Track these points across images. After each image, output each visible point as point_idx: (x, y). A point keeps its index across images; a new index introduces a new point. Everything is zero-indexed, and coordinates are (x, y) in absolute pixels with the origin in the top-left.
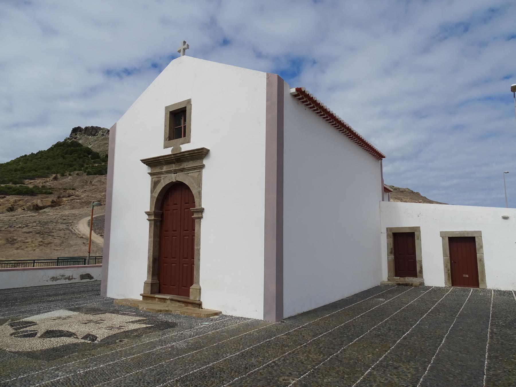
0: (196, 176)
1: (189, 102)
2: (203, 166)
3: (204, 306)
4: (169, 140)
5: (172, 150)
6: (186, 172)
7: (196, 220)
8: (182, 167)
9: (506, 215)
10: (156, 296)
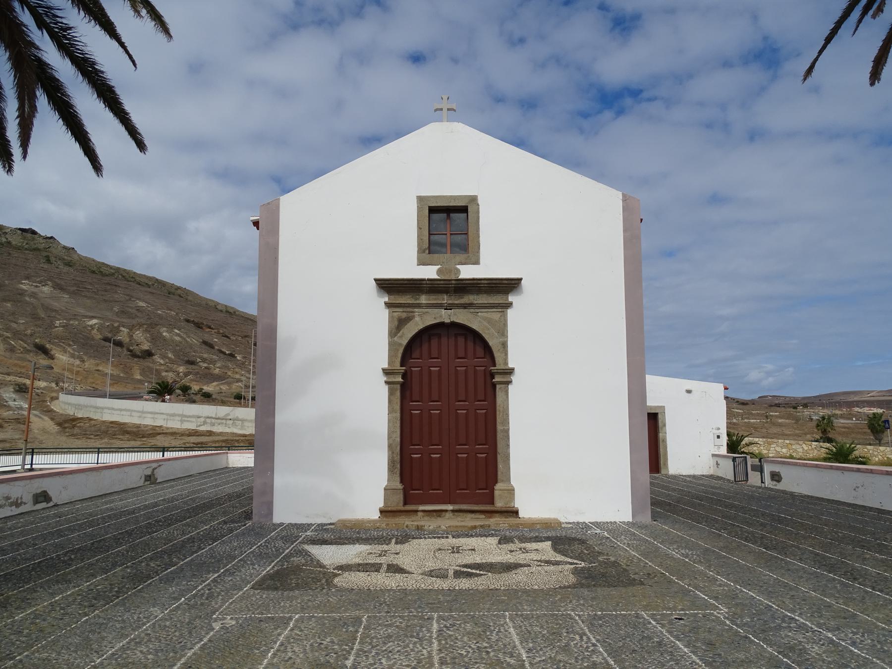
0: (497, 319)
2: (509, 305)
3: (521, 515)
4: (429, 253)
5: (439, 272)
6: (472, 310)
7: (498, 386)
8: (462, 301)
9: (689, 388)
10: (421, 508)
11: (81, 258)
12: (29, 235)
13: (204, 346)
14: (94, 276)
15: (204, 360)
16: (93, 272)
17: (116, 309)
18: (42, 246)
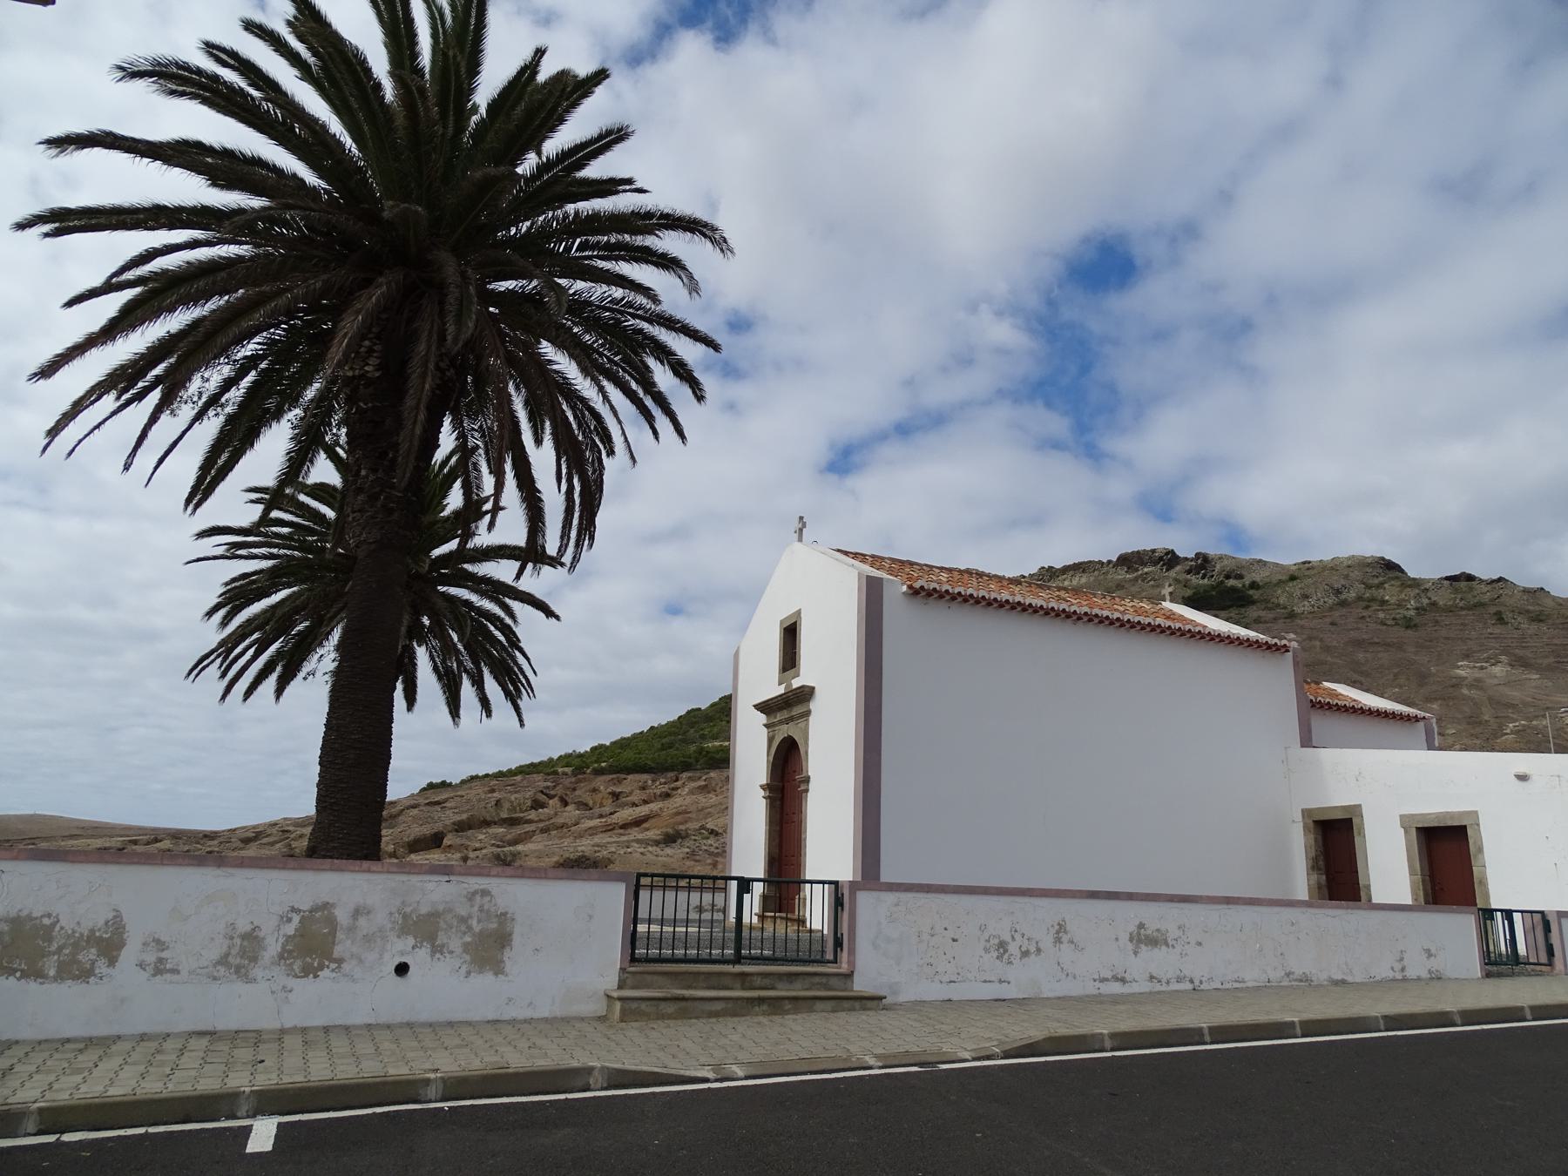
1: (799, 612)
2: (808, 713)
9: (1522, 770)
12: (1463, 584)
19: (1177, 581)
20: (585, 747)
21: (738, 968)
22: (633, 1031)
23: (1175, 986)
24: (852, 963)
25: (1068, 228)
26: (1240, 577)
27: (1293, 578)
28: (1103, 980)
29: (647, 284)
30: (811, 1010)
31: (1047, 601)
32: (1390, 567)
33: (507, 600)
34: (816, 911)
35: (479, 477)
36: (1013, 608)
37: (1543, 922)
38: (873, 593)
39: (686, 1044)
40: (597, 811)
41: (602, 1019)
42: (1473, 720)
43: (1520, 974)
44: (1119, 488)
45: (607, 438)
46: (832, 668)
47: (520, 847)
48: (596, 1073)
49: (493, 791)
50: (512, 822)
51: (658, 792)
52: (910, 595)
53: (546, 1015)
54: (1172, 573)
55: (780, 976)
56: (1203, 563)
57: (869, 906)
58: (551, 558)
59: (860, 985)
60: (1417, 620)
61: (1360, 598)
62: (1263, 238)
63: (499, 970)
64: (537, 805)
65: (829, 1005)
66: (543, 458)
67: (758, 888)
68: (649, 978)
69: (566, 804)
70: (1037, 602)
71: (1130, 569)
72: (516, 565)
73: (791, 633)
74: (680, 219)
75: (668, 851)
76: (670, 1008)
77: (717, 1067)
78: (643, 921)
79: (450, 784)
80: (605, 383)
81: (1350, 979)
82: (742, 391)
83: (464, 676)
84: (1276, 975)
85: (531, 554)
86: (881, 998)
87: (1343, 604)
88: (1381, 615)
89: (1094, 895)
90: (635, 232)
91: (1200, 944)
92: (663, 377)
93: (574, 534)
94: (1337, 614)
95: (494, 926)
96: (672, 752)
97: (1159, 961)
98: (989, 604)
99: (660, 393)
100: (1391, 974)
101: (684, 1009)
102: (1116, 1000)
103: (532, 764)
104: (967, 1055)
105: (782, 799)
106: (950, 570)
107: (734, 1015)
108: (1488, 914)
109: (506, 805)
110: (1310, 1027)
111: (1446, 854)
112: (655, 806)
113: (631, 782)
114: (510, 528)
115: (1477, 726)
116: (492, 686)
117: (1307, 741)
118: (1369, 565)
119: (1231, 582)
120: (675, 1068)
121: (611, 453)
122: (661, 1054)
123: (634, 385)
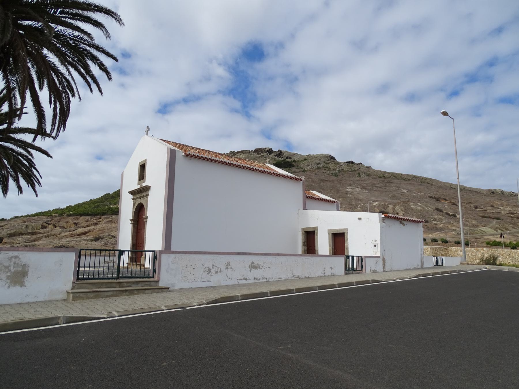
1: (146, 160)
2: (148, 195)
9: (360, 217)
11: (375, 171)
12: (351, 164)
13: (436, 211)
14: (381, 179)
15: (435, 219)
16: (380, 177)
17: (390, 195)
18: (356, 169)
19: (272, 158)
20: (64, 206)
21: (118, 281)
22: (77, 303)
23: (261, 281)
24: (159, 277)
25: (245, 37)
26: (290, 158)
27: (305, 160)
28: (240, 280)
29: (89, 32)
30: (144, 293)
31: (231, 161)
32: (332, 158)
33: (29, 149)
34: (148, 263)
35: (16, 100)
36: (219, 163)
37: (361, 259)
38: (172, 155)
39: (97, 307)
40: (68, 229)
41: (65, 300)
42: (350, 204)
43: (354, 273)
44: (255, 127)
45: (72, 90)
46: (157, 180)
47: (36, 243)
48: (61, 318)
49: (25, 222)
50: (33, 233)
51: (93, 223)
52: (185, 156)
53: (42, 300)
54: (271, 156)
55: (133, 282)
56: (280, 153)
57: (165, 259)
58: (48, 134)
59: (161, 284)
60: (338, 174)
61: (323, 167)
62: (303, 51)
63: (22, 284)
64: (43, 227)
65: (150, 291)
66: (44, 95)
67: (126, 253)
68: (84, 285)
69: (56, 227)
70: (227, 161)
71: (258, 154)
72: (33, 136)
73: (143, 167)
74: (102, 8)
75: (96, 243)
76: (92, 295)
77: (108, 314)
78: (87, 267)
79: (6, 219)
80: (70, 68)
81: (310, 276)
82: (126, 80)
83: (10, 178)
84: (290, 276)
85: (40, 131)
86: (168, 288)
87: (319, 168)
88: (329, 172)
89: (239, 254)
90: (83, 9)
91: (269, 268)
92: (95, 69)
93: (57, 125)
94: (316, 171)
95: (21, 269)
96: (98, 208)
97: (257, 273)
98: (208, 160)
99: (93, 75)
100: (321, 275)
101: (97, 295)
102: (243, 285)
103: (42, 212)
104: (195, 304)
105: (138, 224)
106: (199, 149)
107: (116, 296)
108: (348, 257)
109: (30, 227)
110: (298, 290)
111: (338, 240)
112: (91, 228)
113: (82, 220)
114: (28, 120)
115: (350, 205)
116: (23, 182)
117: (305, 208)
118: (326, 157)
119: (288, 160)
120: (92, 315)
121: (73, 96)
122: (87, 311)
123: (82, 70)
